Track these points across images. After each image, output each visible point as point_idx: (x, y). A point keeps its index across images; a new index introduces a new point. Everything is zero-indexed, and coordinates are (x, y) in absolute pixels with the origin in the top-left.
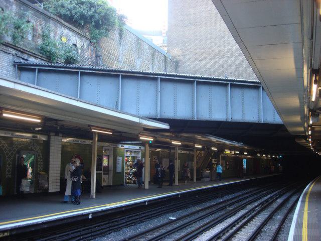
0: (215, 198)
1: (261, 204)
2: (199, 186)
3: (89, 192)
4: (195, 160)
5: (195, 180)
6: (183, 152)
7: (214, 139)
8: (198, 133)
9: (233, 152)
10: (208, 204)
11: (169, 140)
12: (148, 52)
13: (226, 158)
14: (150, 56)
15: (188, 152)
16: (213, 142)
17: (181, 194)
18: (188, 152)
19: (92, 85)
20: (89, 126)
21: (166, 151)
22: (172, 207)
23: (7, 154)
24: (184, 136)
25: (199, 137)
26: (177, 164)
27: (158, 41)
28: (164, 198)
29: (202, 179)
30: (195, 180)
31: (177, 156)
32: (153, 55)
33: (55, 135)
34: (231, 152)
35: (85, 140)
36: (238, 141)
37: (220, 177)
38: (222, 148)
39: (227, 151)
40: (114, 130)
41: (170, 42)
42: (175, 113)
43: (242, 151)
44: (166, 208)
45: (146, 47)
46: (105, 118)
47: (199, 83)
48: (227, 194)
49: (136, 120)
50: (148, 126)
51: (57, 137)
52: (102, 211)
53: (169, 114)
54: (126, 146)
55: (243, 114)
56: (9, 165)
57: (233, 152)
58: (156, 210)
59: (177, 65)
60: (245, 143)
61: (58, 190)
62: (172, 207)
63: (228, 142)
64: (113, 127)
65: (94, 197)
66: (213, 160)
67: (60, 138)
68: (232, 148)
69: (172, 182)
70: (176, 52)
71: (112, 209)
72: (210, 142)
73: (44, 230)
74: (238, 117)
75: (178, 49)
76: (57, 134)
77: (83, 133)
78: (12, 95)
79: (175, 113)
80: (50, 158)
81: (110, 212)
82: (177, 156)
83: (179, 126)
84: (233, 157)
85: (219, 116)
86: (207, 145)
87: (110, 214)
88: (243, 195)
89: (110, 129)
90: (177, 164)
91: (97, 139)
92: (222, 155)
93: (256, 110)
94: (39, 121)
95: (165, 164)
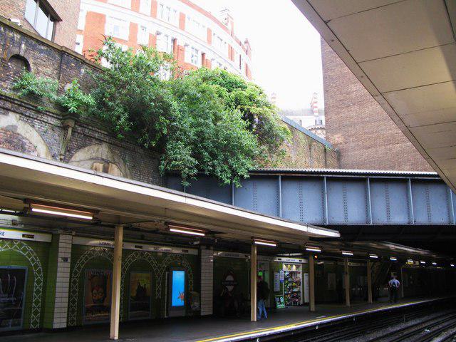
0: (399, 322)
1: (448, 338)
2: (377, 307)
3: (108, 330)
4: (369, 272)
5: (370, 300)
6: (352, 264)
7: (392, 246)
8: (374, 241)
9: (417, 263)
10: (391, 330)
11: (338, 251)
12: (304, 142)
13: (409, 270)
14: (306, 148)
15: (359, 264)
16: (391, 251)
17: (356, 317)
18: (359, 264)
19: (292, 193)
20: (167, 223)
21: (332, 263)
22: (346, 333)
23: (157, 271)
24: (355, 245)
25: (374, 245)
26: (347, 280)
27: (308, 123)
28: (345, 319)
29: (379, 299)
30: (370, 300)
31: (347, 270)
32: (310, 145)
33: (207, 249)
34: (415, 263)
35: (237, 254)
36: (423, 248)
37: (394, 295)
38: (403, 257)
39: (410, 262)
40: (207, 229)
41: (328, 128)
42: (346, 217)
43: (429, 260)
44: (339, 335)
45: (301, 136)
46: (269, 228)
47: (372, 181)
48: (413, 318)
49: (304, 229)
50: (315, 235)
51: (208, 251)
52: (270, 335)
53: (339, 219)
54: (284, 259)
55: (429, 216)
56: (159, 283)
57: (417, 263)
58: (328, 336)
59: (339, 155)
60: (433, 250)
61: (211, 313)
62: (346, 333)
63: (410, 250)
64: (277, 238)
65: (116, 338)
66: (392, 274)
67: (211, 251)
68: (415, 257)
69: (342, 301)
70: (337, 138)
71: (280, 333)
72: (388, 250)
73: (335, 326)
74: (422, 219)
75: (339, 135)
76: (208, 248)
77: (243, 246)
78: (43, 181)
79: (346, 217)
80: (202, 271)
81: (278, 336)
82: (347, 270)
83: (349, 233)
84: (418, 269)
85: (399, 219)
86: (386, 253)
87: (278, 339)
88: (436, 318)
89: (202, 229)
90: (347, 280)
91: (256, 252)
92: (403, 266)
93: (445, 210)
94: (91, 218)
95: (331, 278)
